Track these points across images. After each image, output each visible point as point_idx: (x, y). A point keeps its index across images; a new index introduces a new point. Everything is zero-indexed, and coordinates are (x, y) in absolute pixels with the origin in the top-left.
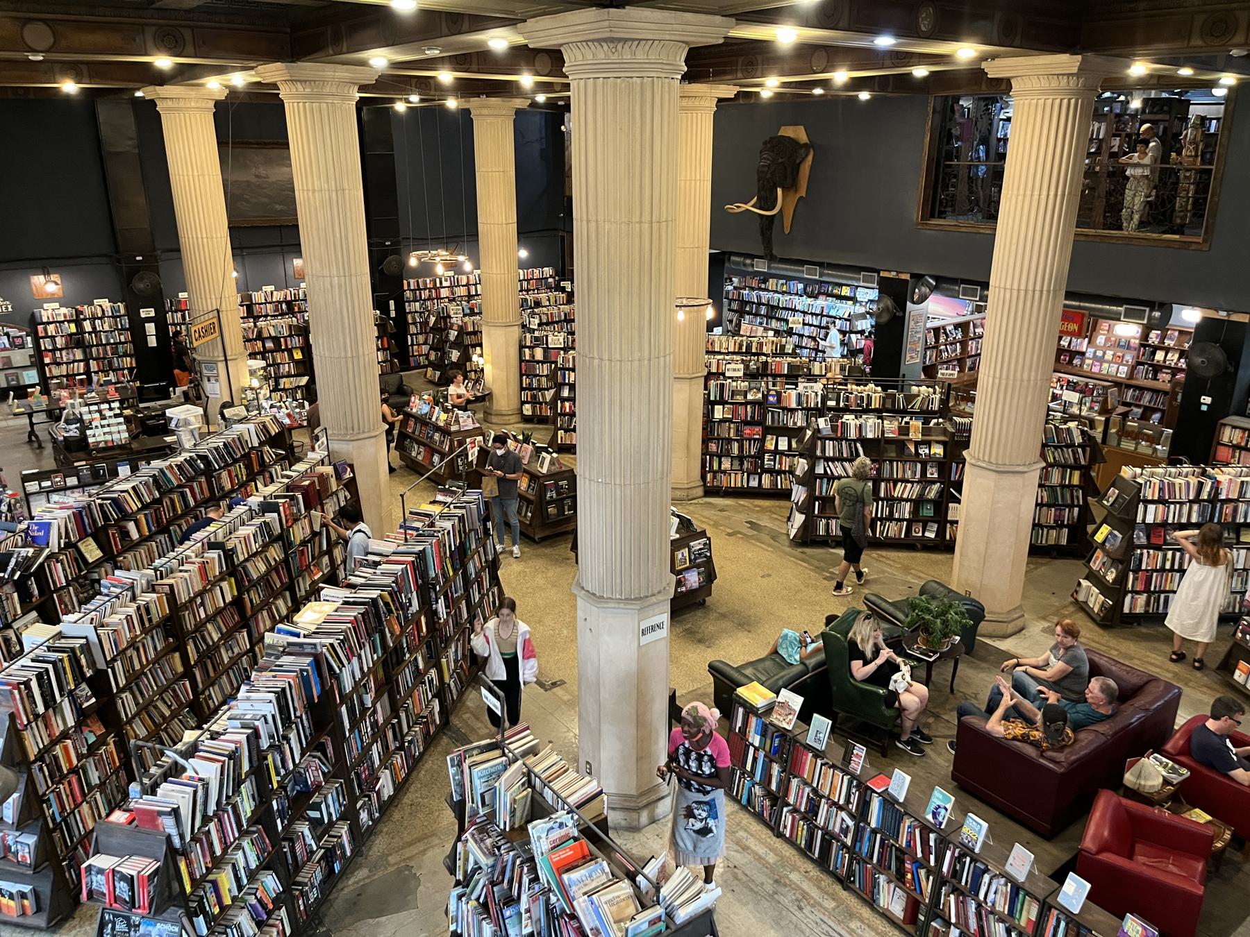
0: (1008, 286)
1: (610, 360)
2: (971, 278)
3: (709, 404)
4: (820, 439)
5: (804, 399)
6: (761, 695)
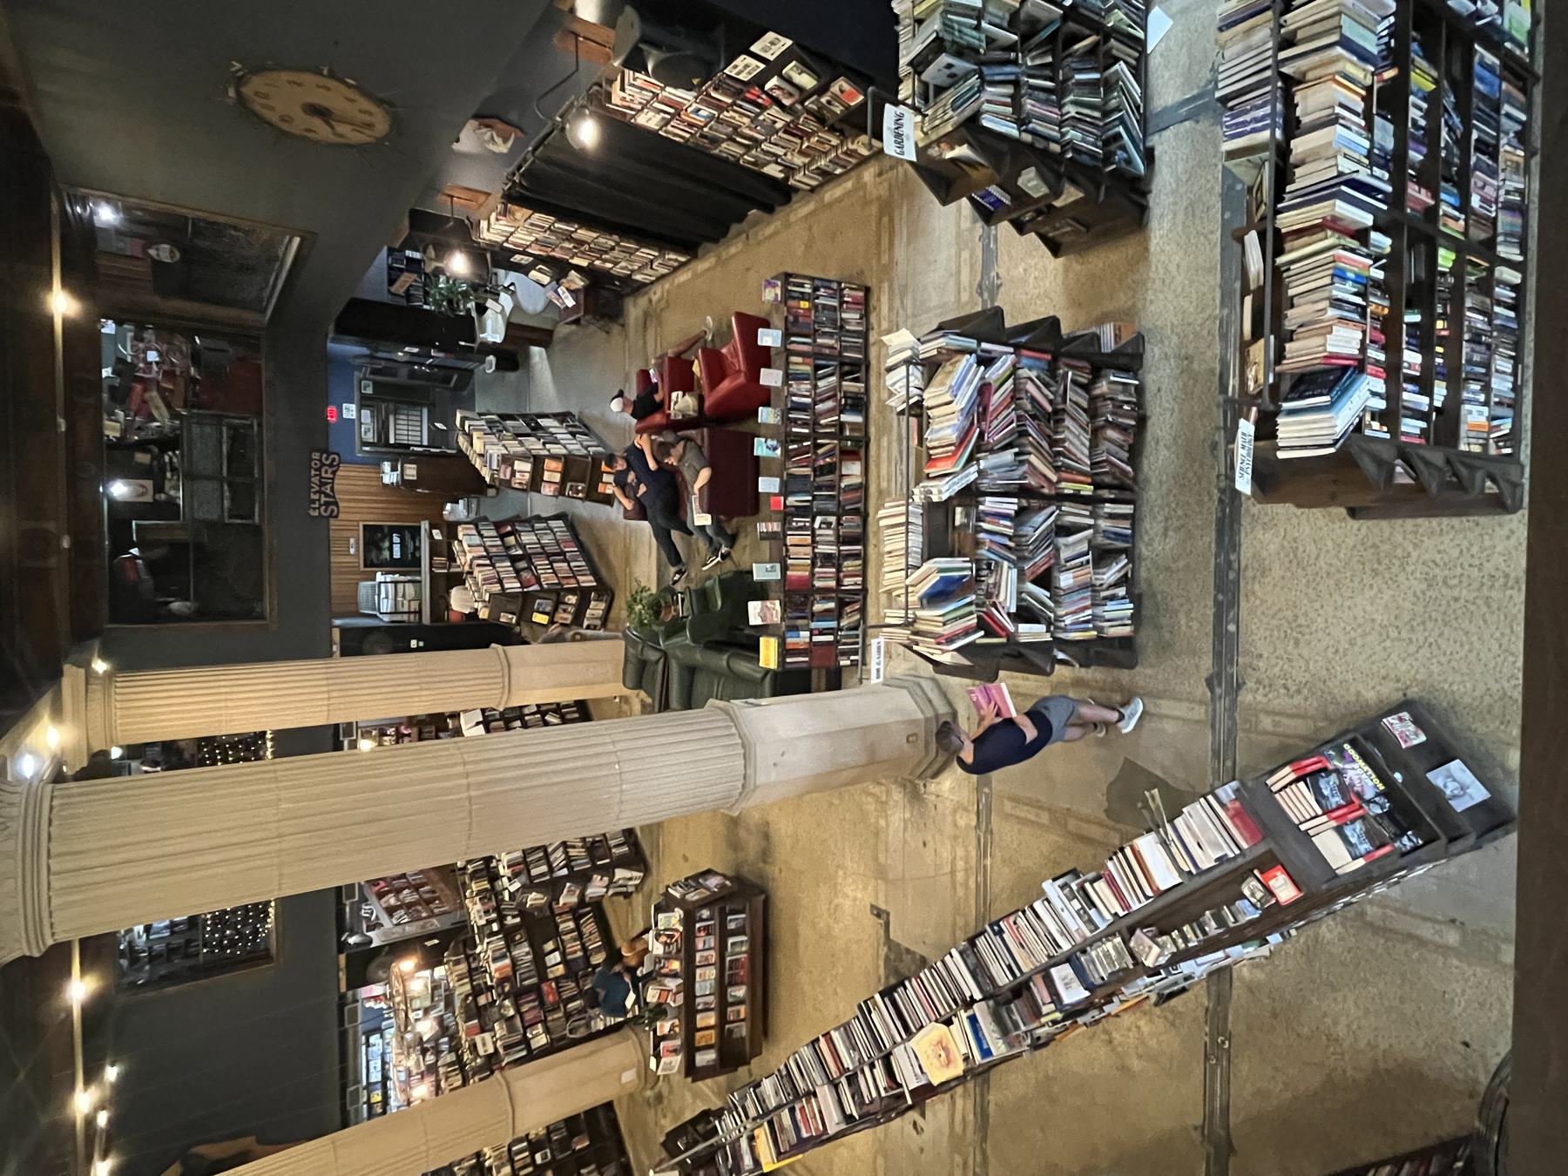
0: (326, 696)
1: (469, 785)
2: (333, 915)
3: (532, 1055)
4: (531, 882)
5: (497, 954)
6: (767, 647)
